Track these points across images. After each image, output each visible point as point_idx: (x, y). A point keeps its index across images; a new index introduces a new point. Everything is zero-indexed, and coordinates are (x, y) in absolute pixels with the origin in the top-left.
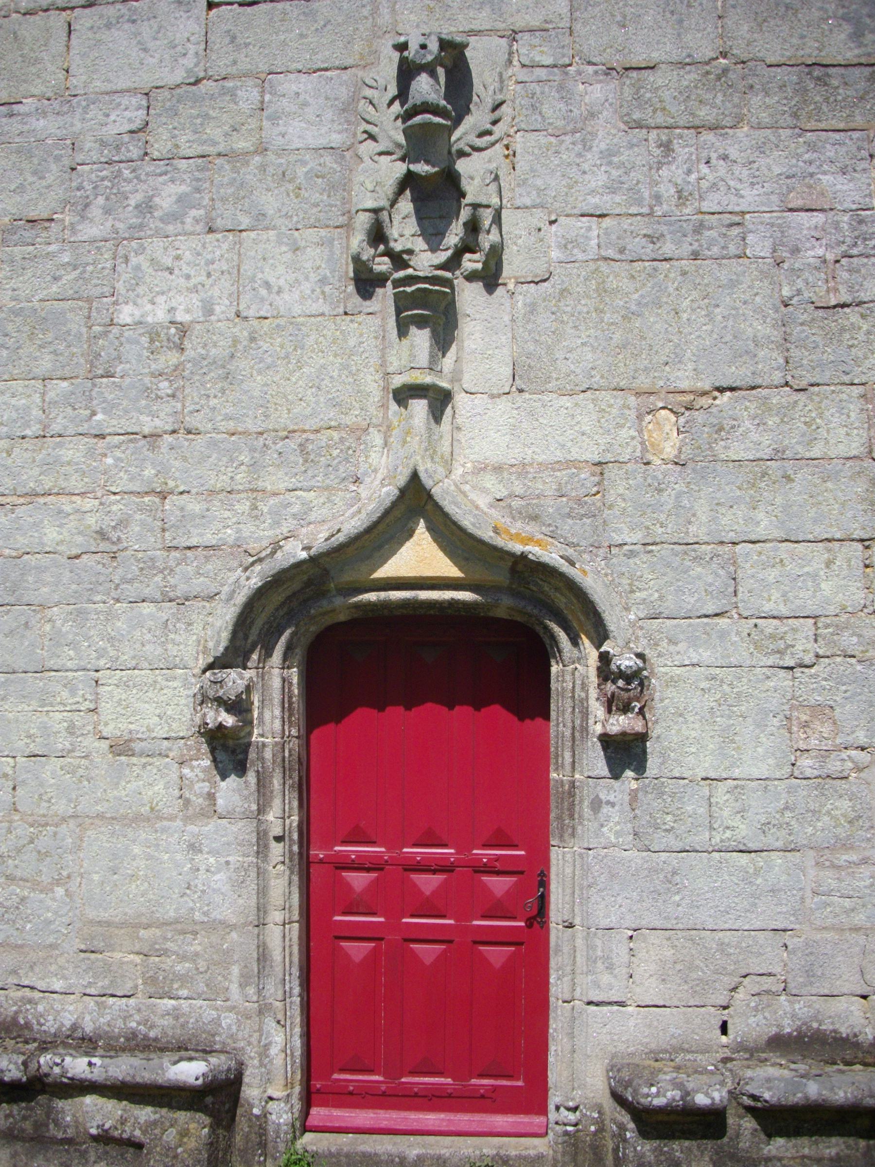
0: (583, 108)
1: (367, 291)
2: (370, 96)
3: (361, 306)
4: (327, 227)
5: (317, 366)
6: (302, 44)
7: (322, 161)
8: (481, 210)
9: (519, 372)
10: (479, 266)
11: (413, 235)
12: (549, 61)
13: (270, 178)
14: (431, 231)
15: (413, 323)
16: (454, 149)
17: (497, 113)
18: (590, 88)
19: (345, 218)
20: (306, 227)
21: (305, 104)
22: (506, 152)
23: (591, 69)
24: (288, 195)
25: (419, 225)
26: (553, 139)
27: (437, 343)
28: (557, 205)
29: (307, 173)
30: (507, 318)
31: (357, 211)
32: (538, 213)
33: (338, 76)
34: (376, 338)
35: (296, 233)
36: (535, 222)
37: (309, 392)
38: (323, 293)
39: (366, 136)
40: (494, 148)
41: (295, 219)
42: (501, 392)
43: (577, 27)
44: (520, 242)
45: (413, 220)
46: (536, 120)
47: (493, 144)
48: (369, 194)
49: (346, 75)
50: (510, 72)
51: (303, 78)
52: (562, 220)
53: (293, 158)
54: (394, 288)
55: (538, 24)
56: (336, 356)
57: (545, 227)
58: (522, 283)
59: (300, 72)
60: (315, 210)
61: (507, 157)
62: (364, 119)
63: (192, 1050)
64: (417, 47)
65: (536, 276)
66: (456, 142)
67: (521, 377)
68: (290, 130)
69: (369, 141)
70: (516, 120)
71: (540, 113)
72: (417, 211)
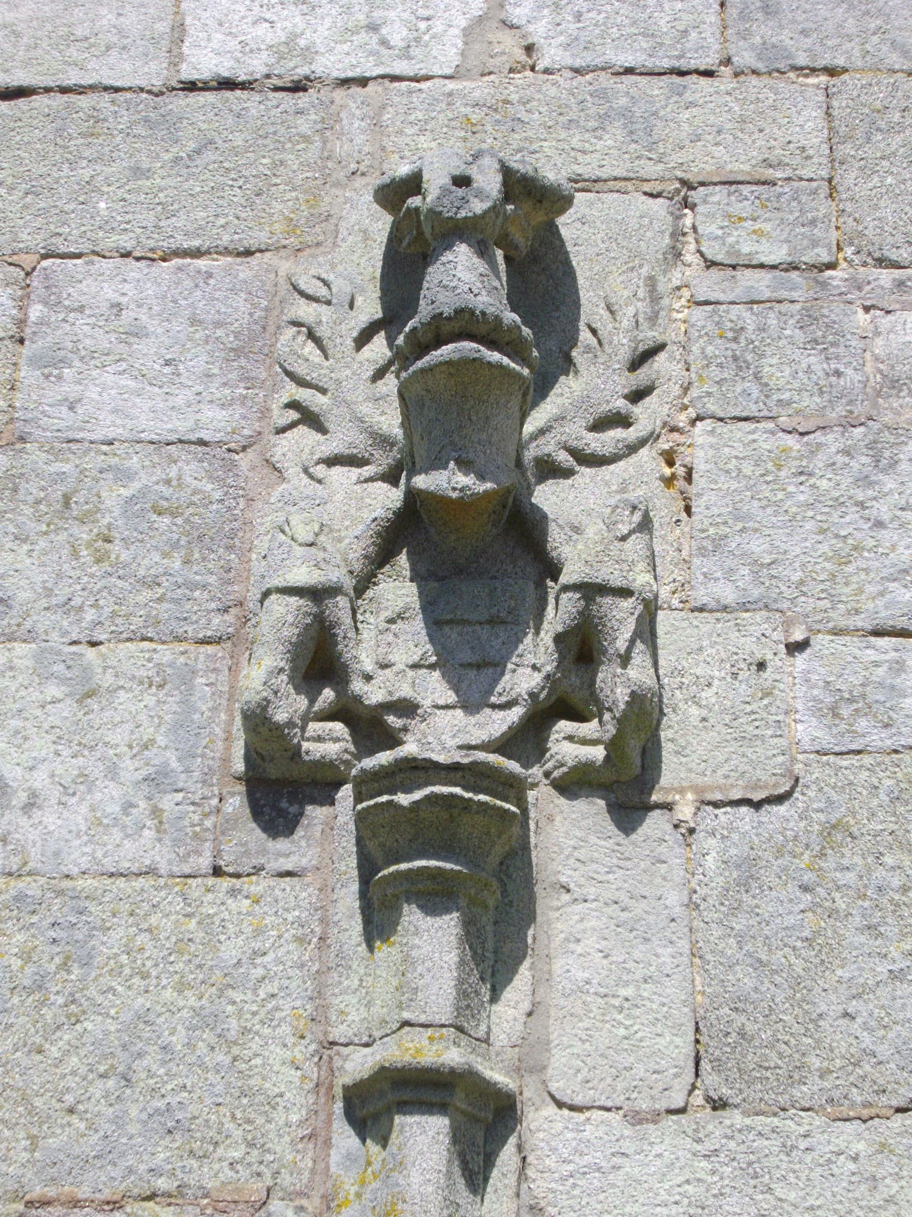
0: (869, 368)
1: (282, 813)
2: (310, 319)
3: (264, 852)
4: (179, 639)
5: (126, 1016)
6: (138, 191)
7: (173, 472)
8: (608, 600)
9: (712, 1048)
10: (598, 753)
11: (415, 666)
12: (778, 254)
13: (28, 511)
14: (466, 656)
15: (414, 896)
16: (530, 454)
17: (643, 375)
18: (885, 322)
19: (229, 618)
20: (118, 638)
21: (137, 332)
22: (668, 471)
23: (886, 277)
24: (75, 554)
25: (432, 640)
26: (791, 441)
27: (478, 958)
28: (806, 604)
29: (130, 501)
30: (674, 899)
31: (266, 594)
32: (756, 621)
33: (228, 271)
34: (300, 940)
35: (91, 654)
36: (751, 647)
37: (97, 1089)
38: (156, 812)
39: (293, 415)
40: (633, 459)
41: (90, 615)
42: (661, 1105)
43: (848, 178)
44: (707, 695)
45: (418, 625)
46: (746, 393)
47: (632, 449)
48: (299, 551)
49: (246, 270)
50: (676, 277)
51: (134, 269)
52: (821, 642)
53: (93, 462)
54: (358, 799)
55: (746, 167)
56: (181, 988)
57: (777, 659)
58: (716, 805)
59: (126, 255)
60: (146, 595)
61: (669, 481)
62: (289, 374)
63: (228, 748)
64: (447, 181)
65: (755, 787)
66: (534, 437)
67: (718, 1065)
68: (93, 393)
69: (302, 430)
70: (694, 393)
71: (757, 377)
72: (428, 605)
